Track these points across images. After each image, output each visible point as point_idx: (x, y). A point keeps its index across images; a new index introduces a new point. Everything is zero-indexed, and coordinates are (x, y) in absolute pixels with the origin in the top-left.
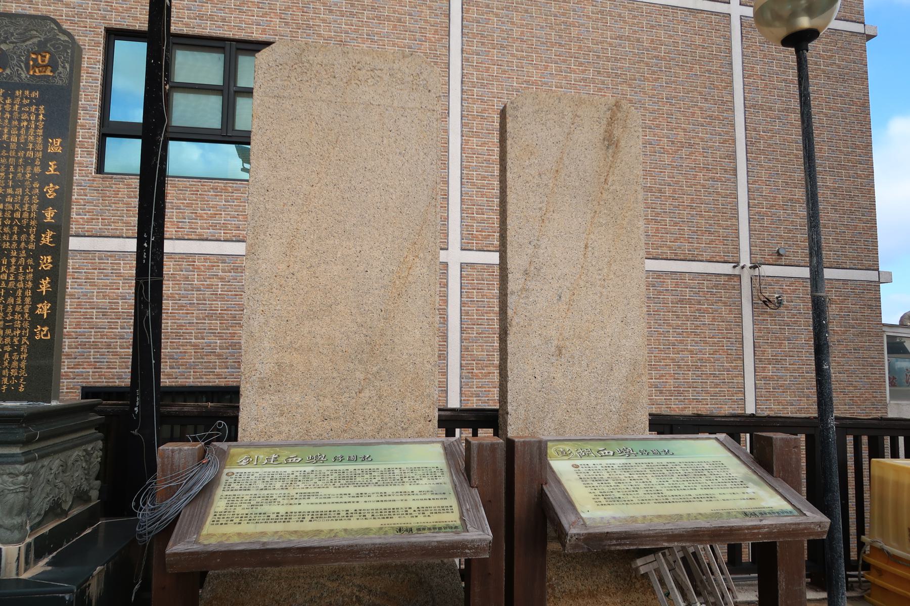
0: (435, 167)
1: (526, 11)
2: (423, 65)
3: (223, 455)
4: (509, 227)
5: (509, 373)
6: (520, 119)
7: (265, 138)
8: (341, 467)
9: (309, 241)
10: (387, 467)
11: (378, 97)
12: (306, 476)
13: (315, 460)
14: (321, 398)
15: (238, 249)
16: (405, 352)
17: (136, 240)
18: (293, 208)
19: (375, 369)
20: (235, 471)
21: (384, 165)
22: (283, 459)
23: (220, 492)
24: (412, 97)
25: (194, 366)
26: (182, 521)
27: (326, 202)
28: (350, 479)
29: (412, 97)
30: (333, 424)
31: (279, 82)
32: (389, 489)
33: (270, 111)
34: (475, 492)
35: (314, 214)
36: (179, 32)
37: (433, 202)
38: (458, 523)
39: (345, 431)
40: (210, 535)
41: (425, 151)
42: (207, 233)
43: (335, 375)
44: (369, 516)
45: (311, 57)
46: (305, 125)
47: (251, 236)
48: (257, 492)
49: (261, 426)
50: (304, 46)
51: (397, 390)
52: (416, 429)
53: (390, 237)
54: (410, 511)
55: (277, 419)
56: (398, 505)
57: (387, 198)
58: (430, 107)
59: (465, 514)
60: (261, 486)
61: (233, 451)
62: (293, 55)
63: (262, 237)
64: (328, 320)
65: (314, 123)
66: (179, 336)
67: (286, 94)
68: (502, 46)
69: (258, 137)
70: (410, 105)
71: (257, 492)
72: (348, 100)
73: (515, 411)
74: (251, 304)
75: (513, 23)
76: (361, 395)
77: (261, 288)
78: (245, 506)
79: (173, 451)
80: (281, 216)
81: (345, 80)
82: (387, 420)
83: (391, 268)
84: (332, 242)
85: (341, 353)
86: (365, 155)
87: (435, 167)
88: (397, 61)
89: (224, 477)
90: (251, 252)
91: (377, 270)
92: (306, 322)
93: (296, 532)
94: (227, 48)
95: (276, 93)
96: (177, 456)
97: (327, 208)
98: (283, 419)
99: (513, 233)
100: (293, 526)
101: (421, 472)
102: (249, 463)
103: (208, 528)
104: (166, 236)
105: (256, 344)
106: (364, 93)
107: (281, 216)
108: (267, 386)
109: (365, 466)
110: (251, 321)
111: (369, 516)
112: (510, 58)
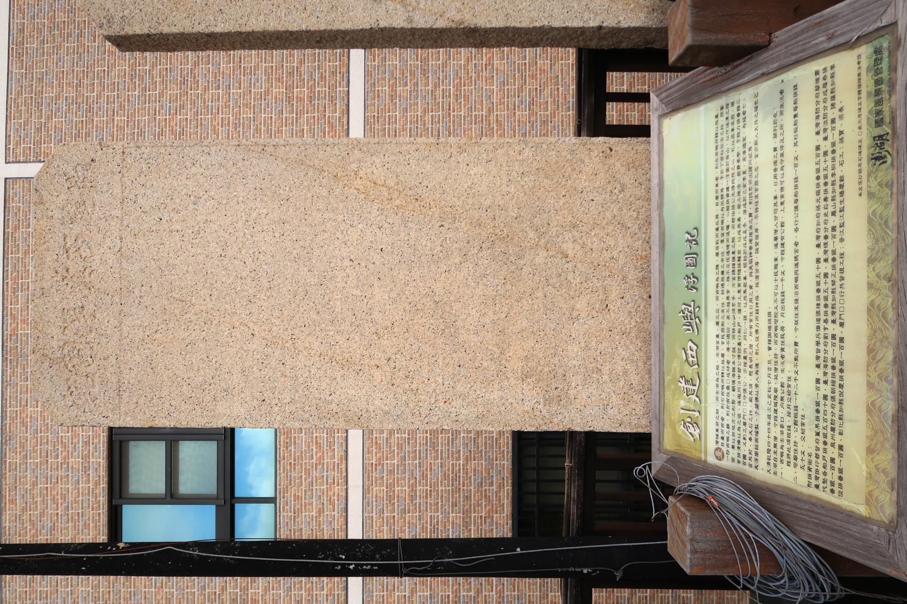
0: (213, 149)
1: (40, 80)
2: (52, 171)
3: (685, 465)
4: (304, 27)
5: (537, 24)
6: (126, 12)
7: (184, 407)
8: (710, 278)
9: (338, 338)
10: (712, 200)
11: (108, 241)
12: (725, 334)
13: (692, 318)
14: (575, 314)
15: (356, 437)
16: (505, 189)
17: (349, 578)
18: (289, 362)
19: (532, 234)
20: (711, 446)
21: (215, 227)
22: (690, 372)
23: (761, 473)
24: (105, 188)
25: (490, 461)
26: (819, 540)
27: (277, 313)
28: (740, 264)
29: (105, 188)
30: (614, 295)
31: (96, 390)
32: (767, 190)
33: (141, 402)
34: (780, 35)
35: (296, 332)
36: (106, 492)
37: (270, 149)
38: (865, 51)
39: (624, 278)
40: (869, 499)
41: (188, 164)
42: (338, 451)
43: (540, 294)
44: (834, 221)
45: (54, 344)
46: (160, 349)
47: (332, 422)
48: (763, 413)
49: (615, 400)
50: (38, 355)
51: (563, 200)
52: (623, 170)
53: (326, 215)
54: (826, 146)
55: (606, 377)
56: (807, 172)
57: (265, 221)
58: (118, 158)
59: (842, 40)
60: (749, 406)
61: (669, 444)
62: (52, 372)
63: (334, 406)
64: (457, 306)
65: (158, 336)
66: (456, 478)
67: (114, 379)
68: (89, 110)
69: (182, 417)
70: (117, 190)
71: (763, 413)
72: (117, 285)
73: (596, 14)
74: (435, 419)
75: (58, 97)
76: (571, 253)
77: (411, 405)
78: (796, 436)
79: (694, 552)
80: (301, 380)
81: (86, 292)
82: (608, 215)
83: (375, 212)
84: (338, 303)
85: (508, 286)
86: (201, 258)
87: (213, 149)
88: (50, 214)
89: (726, 464)
90: (357, 420)
91: (379, 233)
92: (461, 338)
93: (870, 350)
94: (121, 438)
95: (114, 394)
96: (702, 546)
97: (286, 312)
98: (606, 369)
99: (314, 20)
100: (854, 354)
101: (728, 144)
102: (695, 424)
103: (853, 500)
104: (344, 537)
105: (495, 410)
106: (103, 262)
107: (301, 380)
108: (556, 393)
109: (709, 238)
110: (461, 418)
111: (834, 221)
112: (103, 101)
